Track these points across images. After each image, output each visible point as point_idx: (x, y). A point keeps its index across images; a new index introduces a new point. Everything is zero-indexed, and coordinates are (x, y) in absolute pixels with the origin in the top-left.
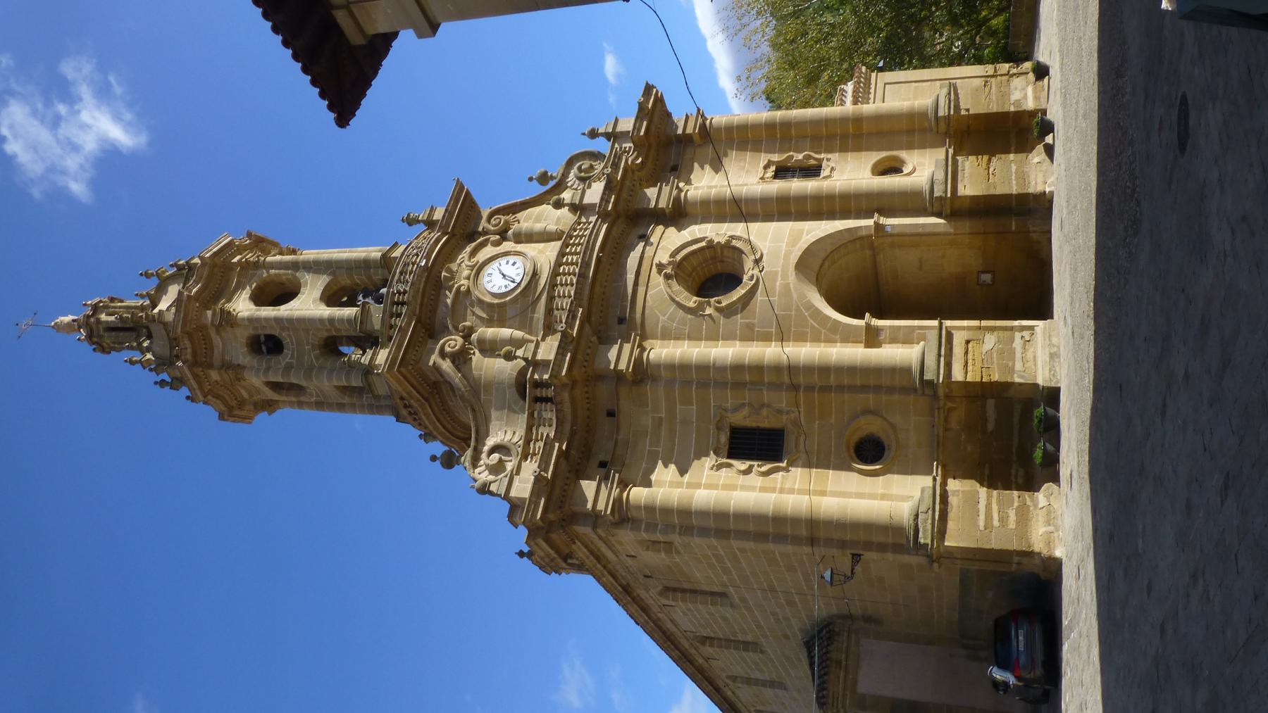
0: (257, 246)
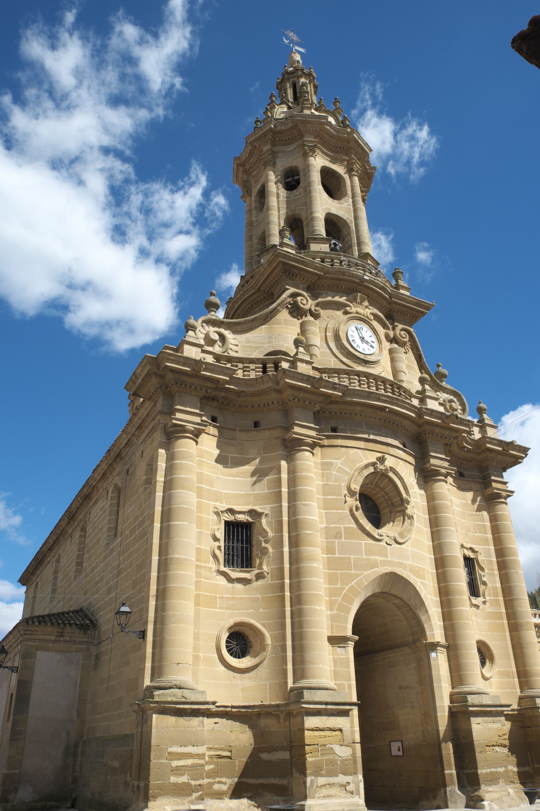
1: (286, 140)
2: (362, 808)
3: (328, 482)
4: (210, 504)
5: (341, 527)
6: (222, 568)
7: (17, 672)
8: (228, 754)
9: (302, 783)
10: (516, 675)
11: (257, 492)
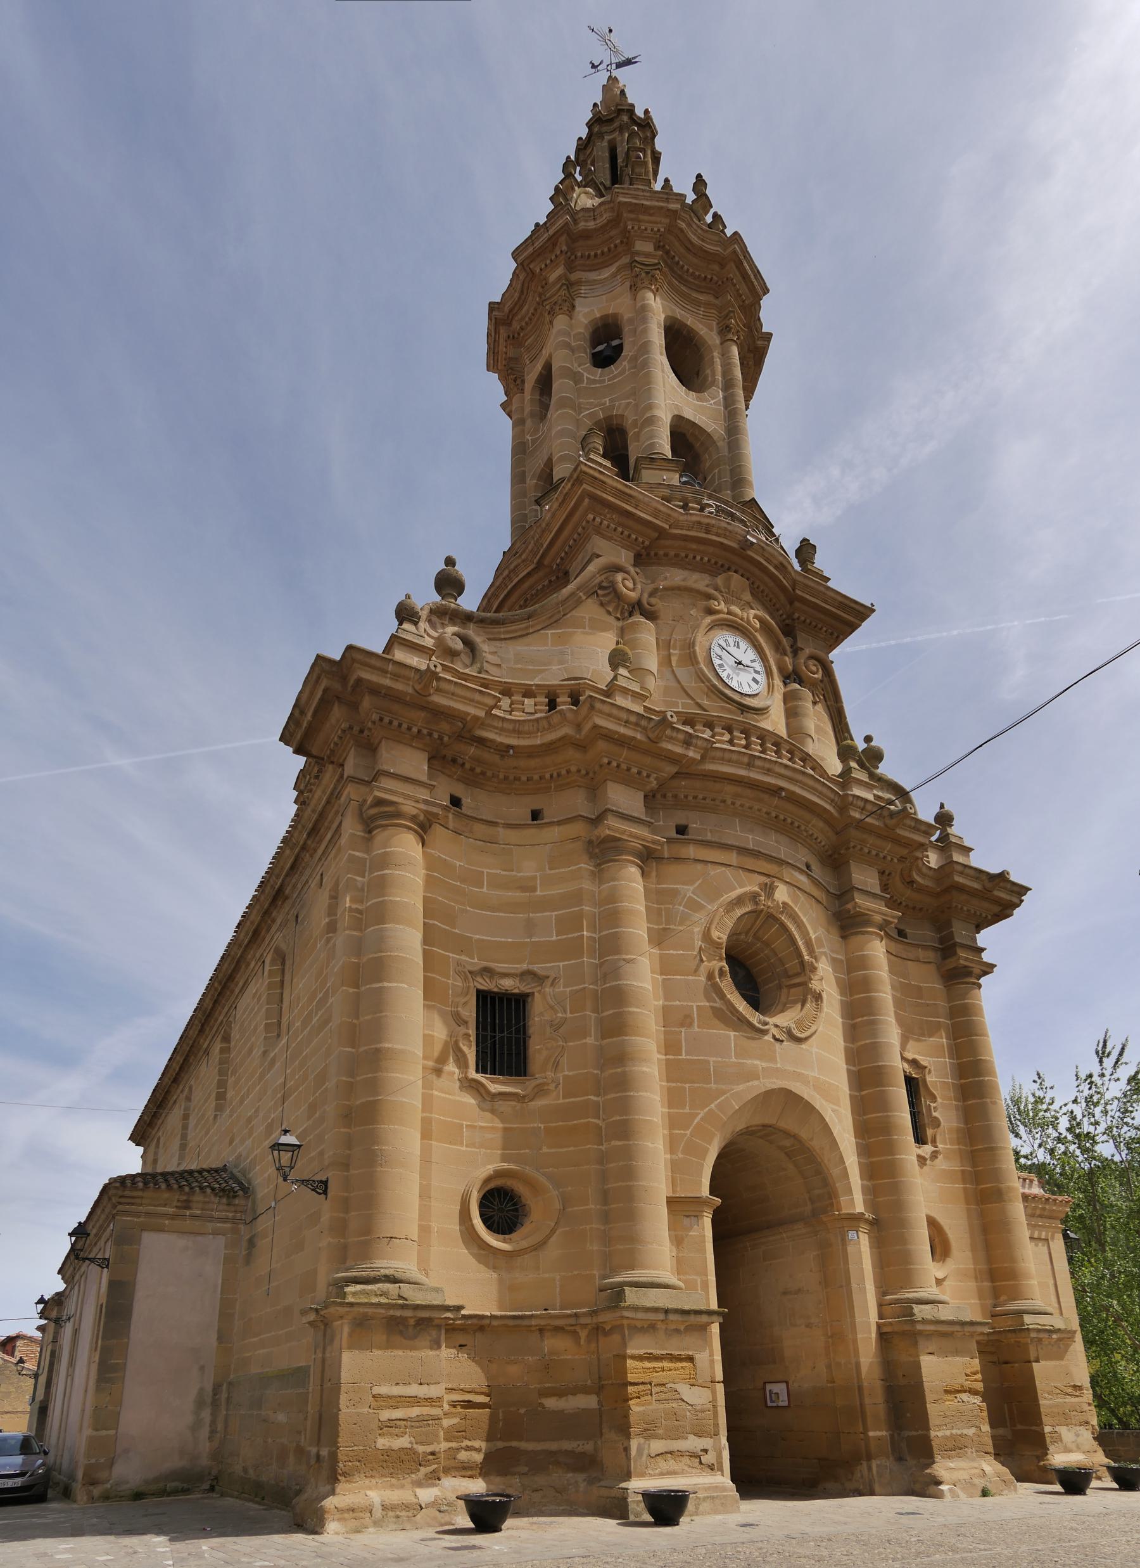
1: (596, 255)
3: (669, 925)
5: (693, 1006)
7: (107, 1267)
9: (622, 1450)
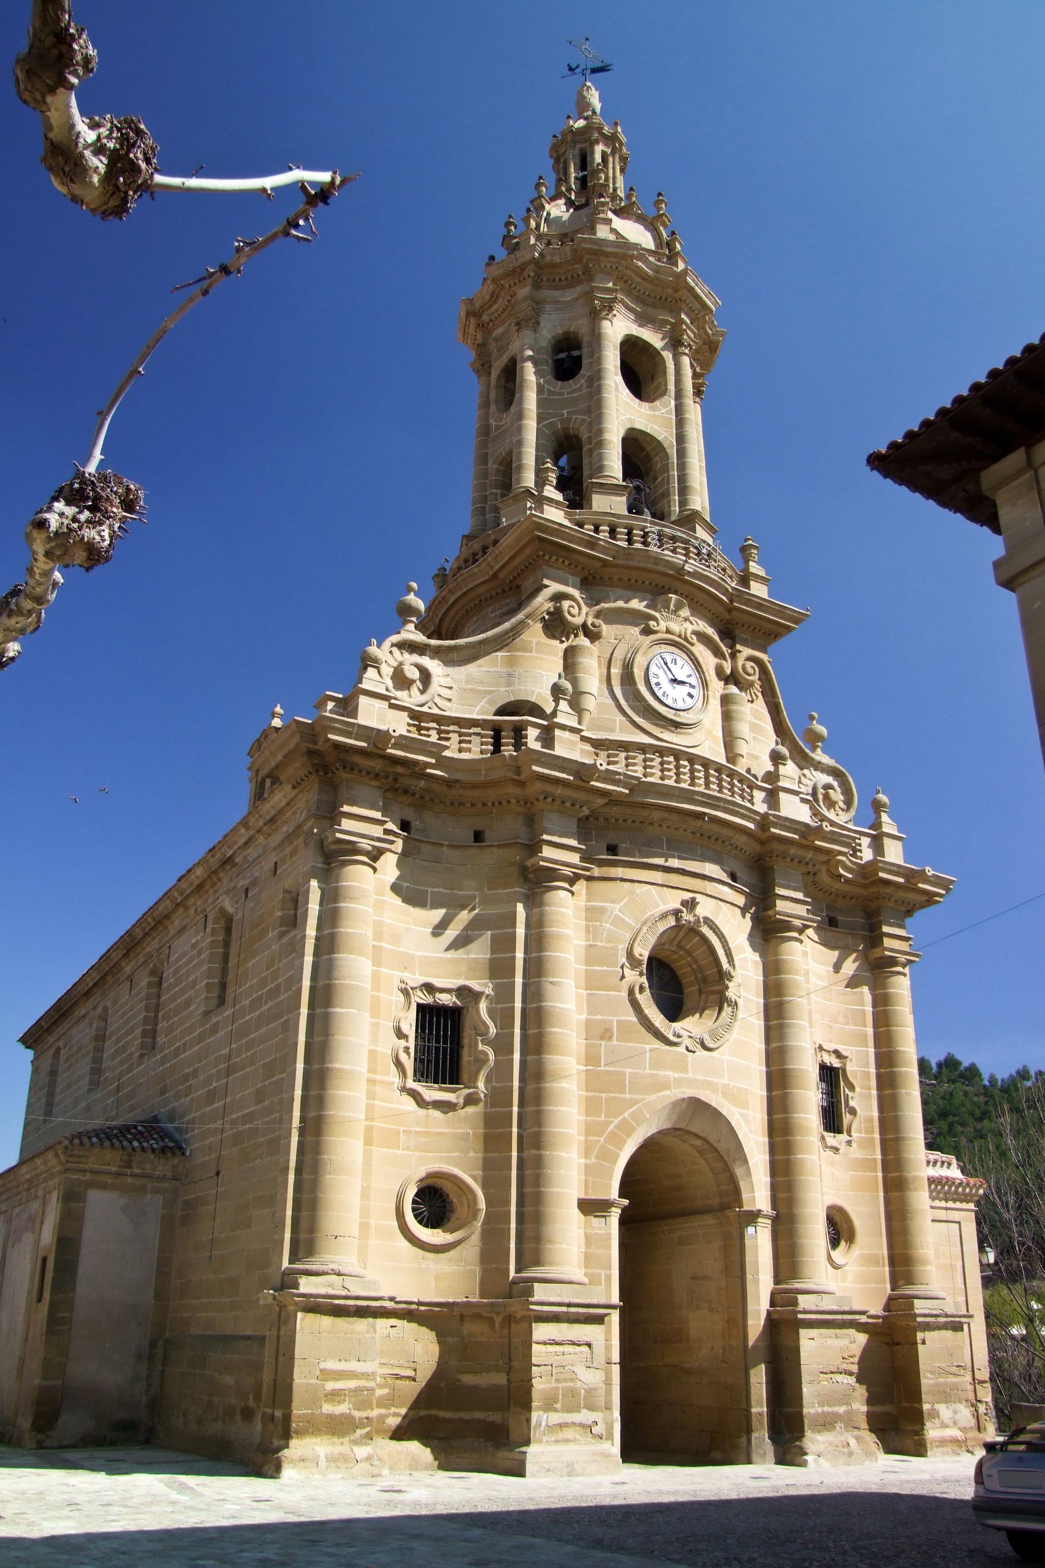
0: (704, 343)
2: (616, 1459)
4: (393, 975)
6: (411, 1084)
8: (411, 1373)
10: (886, 1261)
11: (474, 956)
